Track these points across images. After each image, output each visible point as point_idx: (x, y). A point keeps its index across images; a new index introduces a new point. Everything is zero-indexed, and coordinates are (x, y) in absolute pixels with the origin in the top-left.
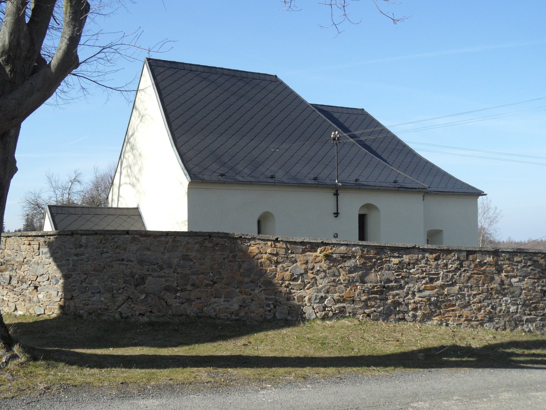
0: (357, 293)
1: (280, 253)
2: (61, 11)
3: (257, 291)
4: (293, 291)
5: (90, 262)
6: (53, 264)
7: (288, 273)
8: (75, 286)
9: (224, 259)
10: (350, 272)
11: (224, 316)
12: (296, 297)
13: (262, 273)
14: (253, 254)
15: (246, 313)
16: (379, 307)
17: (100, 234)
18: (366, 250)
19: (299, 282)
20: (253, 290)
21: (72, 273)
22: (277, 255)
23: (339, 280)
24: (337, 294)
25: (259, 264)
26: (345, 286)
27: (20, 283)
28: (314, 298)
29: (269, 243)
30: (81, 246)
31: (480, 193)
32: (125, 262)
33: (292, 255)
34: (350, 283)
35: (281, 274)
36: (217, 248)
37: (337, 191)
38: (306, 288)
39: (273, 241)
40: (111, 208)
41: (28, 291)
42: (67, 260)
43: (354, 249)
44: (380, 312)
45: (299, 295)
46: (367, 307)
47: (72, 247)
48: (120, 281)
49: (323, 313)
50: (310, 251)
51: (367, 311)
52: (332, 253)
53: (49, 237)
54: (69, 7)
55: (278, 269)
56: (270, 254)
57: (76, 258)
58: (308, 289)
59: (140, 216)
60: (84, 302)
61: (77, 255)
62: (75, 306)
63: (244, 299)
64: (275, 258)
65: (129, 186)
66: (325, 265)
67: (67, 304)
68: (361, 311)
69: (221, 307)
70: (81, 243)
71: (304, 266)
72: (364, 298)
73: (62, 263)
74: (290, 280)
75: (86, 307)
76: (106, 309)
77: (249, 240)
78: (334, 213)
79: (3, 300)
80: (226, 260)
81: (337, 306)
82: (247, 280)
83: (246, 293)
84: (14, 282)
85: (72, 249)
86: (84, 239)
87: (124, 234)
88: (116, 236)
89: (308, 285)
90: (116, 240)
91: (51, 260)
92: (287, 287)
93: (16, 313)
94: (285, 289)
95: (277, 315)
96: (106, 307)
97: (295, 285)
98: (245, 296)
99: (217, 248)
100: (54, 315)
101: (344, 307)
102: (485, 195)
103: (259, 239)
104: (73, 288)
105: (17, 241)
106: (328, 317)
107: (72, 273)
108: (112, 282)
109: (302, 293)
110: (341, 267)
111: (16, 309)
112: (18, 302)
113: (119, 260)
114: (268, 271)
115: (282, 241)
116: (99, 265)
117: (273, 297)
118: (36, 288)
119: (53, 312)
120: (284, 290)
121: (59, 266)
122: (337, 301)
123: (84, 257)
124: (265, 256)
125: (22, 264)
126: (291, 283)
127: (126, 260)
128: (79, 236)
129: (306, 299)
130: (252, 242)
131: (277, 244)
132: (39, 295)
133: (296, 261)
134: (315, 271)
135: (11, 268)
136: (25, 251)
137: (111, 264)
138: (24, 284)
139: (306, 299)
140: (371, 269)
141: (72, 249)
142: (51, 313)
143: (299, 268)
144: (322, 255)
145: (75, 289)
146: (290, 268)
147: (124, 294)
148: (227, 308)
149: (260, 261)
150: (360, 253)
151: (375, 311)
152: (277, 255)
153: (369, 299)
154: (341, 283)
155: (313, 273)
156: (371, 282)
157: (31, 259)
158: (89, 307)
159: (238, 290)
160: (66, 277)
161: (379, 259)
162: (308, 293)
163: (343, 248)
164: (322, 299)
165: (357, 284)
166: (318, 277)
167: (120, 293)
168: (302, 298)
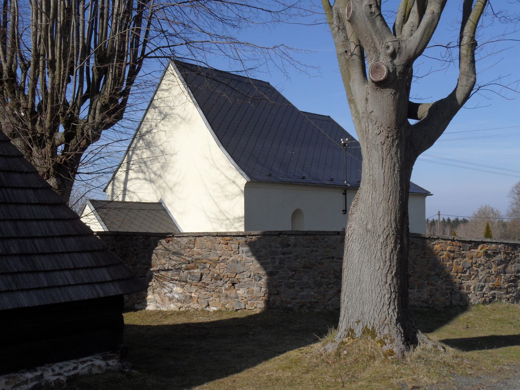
0: (502, 282)
1: (455, 250)
2: (9, 2)
3: (439, 283)
4: (463, 282)
5: (299, 260)
6: (256, 262)
7: (460, 266)
8: (281, 282)
9: (417, 256)
10: (498, 265)
11: (418, 304)
12: (465, 287)
13: (442, 268)
14: (437, 252)
15: (433, 301)
16: (514, 293)
17: (310, 235)
18: (506, 246)
19: (467, 274)
20: (437, 282)
21: (279, 270)
22: (453, 252)
23: (492, 272)
24: (491, 283)
25: (442, 260)
26: (495, 277)
27: (213, 280)
28: (477, 287)
29: (449, 242)
30: (289, 245)
31: (427, 194)
32: (335, 260)
33: (463, 252)
34: (498, 274)
35: (454, 267)
36: (412, 247)
37: (345, 191)
38: (472, 279)
39: (451, 240)
40: (118, 202)
41: (223, 288)
42: (273, 258)
43: (500, 246)
44: (514, 297)
45: (467, 285)
46: (508, 293)
47: (278, 246)
48: (330, 276)
49: (483, 299)
50: (474, 248)
51: (507, 296)
52: (488, 250)
53: (251, 237)
54: (470, 51)
55: (454, 264)
56: (449, 251)
57: (282, 256)
58: (473, 280)
59: (165, 210)
60: (292, 296)
61: (284, 254)
62: (282, 301)
63: (431, 289)
64: (452, 254)
65: (144, 181)
66: (483, 260)
67: (271, 299)
68: (504, 296)
69: (415, 296)
70: (289, 242)
71: (470, 261)
72: (506, 286)
73: (266, 261)
74: (462, 273)
75: (293, 301)
76: (317, 302)
77: (435, 239)
78: (343, 211)
79: (191, 297)
80: (419, 257)
81: (491, 293)
82: (433, 273)
83: (432, 285)
84: (205, 279)
85: (278, 248)
86: (292, 239)
87: (335, 235)
88: (327, 236)
89: (473, 277)
90: (326, 239)
91: (253, 258)
92: (460, 278)
93: (207, 309)
94: (459, 280)
95: (453, 301)
96: (316, 300)
97: (465, 276)
98: (431, 287)
99: (412, 247)
100: (258, 311)
101: (495, 294)
102: (432, 195)
103: (442, 239)
104: (280, 284)
105: (211, 241)
106: (486, 302)
107: (279, 270)
108: (322, 277)
109: (469, 283)
110: (493, 261)
111: (208, 305)
112: (211, 299)
113: (329, 258)
114: (447, 266)
115: (457, 240)
116: (310, 262)
117: (450, 287)
118: (233, 284)
119: (257, 306)
120: (458, 280)
121: (262, 264)
122: (492, 289)
123: (292, 255)
124: (445, 253)
125: (217, 262)
126: (462, 275)
127: (336, 258)
128: (285, 236)
129: (472, 288)
130: (437, 241)
131: (453, 242)
132: (238, 292)
133: (465, 257)
134: (477, 264)
135: (202, 266)
136: (221, 250)
137: (322, 261)
138: (219, 281)
139: (472, 288)
140: (509, 263)
141: (278, 248)
142: (253, 307)
143: (468, 261)
144: (482, 251)
145: (282, 285)
146: (461, 263)
147: (335, 288)
148: (420, 298)
149: (442, 257)
150: (503, 250)
151: (512, 296)
152: (453, 252)
153: (509, 287)
154: (493, 274)
155: (476, 267)
156: (509, 273)
157: (229, 258)
158: (297, 301)
159: (426, 282)
160: (270, 274)
161: (514, 254)
162: (472, 283)
163: (494, 245)
164: (483, 287)
165: (502, 274)
166: (479, 270)
167: (331, 288)
168: (468, 287)
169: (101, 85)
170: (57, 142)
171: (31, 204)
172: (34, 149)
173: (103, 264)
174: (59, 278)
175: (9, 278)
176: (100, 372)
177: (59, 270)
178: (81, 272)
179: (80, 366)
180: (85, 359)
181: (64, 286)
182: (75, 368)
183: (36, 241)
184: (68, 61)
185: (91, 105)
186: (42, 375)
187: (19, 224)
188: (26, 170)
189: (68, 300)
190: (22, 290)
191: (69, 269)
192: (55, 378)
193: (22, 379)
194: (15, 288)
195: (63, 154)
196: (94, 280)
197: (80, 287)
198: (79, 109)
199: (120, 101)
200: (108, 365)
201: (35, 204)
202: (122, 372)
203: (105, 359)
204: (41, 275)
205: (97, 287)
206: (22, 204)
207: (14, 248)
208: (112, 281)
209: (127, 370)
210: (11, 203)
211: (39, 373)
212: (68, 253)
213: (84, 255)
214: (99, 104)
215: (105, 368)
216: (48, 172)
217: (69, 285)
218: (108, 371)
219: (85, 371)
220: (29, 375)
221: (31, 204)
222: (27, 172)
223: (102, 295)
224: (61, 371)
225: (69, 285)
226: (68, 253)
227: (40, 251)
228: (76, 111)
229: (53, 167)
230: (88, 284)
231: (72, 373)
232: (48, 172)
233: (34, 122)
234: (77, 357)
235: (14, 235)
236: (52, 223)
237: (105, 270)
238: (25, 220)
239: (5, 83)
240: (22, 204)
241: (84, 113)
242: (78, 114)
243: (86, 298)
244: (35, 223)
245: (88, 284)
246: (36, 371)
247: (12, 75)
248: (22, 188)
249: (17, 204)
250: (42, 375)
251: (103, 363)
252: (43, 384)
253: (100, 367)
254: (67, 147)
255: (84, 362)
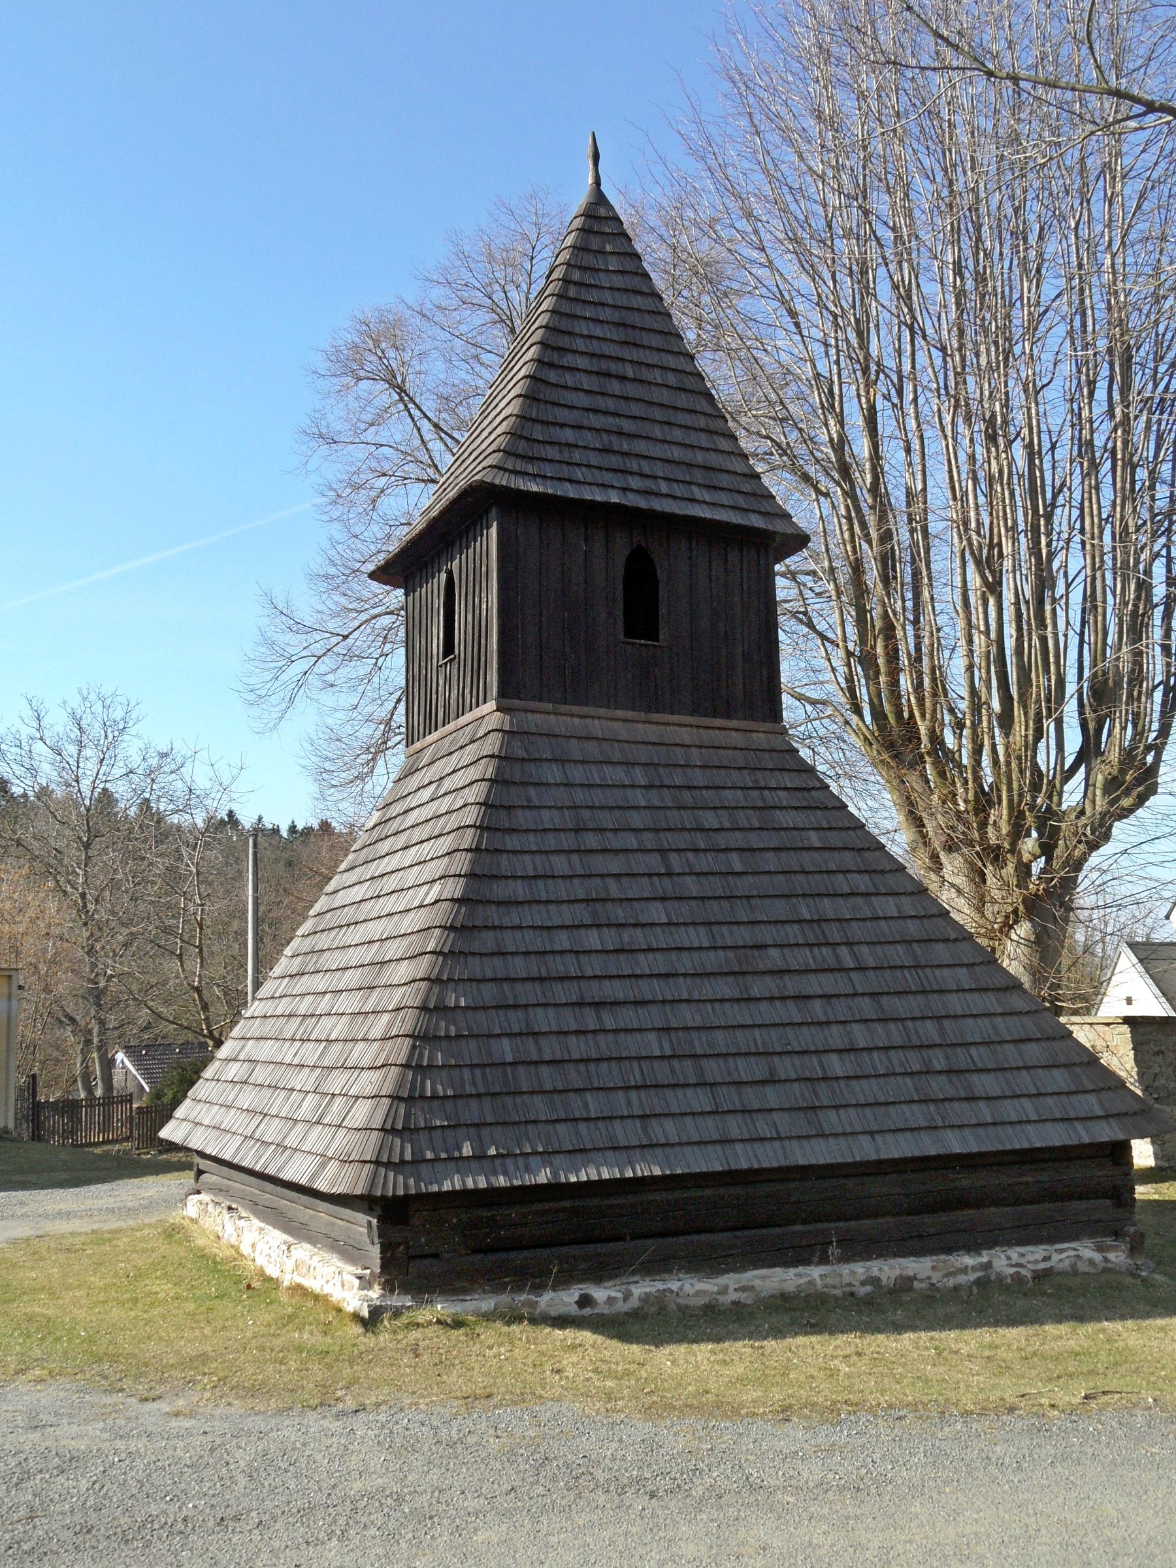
169: (1104, 739)
170: (1026, 857)
171: (964, 990)
172: (989, 870)
173: (1090, 1087)
174: (1010, 1108)
175: (932, 1107)
176: (1092, 1271)
177: (1011, 1097)
178: (1050, 1101)
179: (1056, 1257)
180: (1065, 1245)
181: (1020, 1122)
182: (1047, 1259)
183: (973, 1050)
184: (1032, 713)
185: (1087, 779)
186: (990, 1262)
187: (946, 1023)
188: (953, 936)
189: (1026, 1146)
190: (952, 1127)
191: (1029, 1096)
192: (1012, 1270)
193: (958, 1265)
194: (940, 1123)
195: (1040, 878)
196: (1072, 1115)
197: (1049, 1125)
198: (1060, 794)
199: (1150, 759)
200: (1106, 1260)
201: (971, 990)
202: (1134, 1276)
203: (1100, 1249)
204: (982, 1105)
205: (1078, 1126)
206: (950, 991)
207: (938, 1060)
208: (1106, 1117)
209: (1144, 1274)
210: (933, 992)
211: (985, 1259)
212: (1026, 1068)
213: (1055, 1072)
214: (1100, 777)
215: (1101, 1265)
216: (1015, 912)
217: (1029, 1122)
218: (1106, 1270)
219: (1066, 1264)
220: (969, 1260)
221: (964, 990)
222: (956, 940)
223: (1086, 1140)
224: (1023, 1261)
225: (1029, 1122)
226: (1026, 1068)
227: (980, 1065)
228: (1055, 799)
229: (1024, 901)
230: (1062, 1120)
231: (1042, 1266)
232: (1015, 912)
233: (983, 825)
234: (1051, 1240)
235: (938, 1042)
236: (998, 1021)
237: (1092, 1098)
238: (955, 1017)
239: (927, 758)
240: (950, 991)
241: (1073, 794)
242: (1060, 804)
243: (1058, 1144)
244: (970, 1022)
245: (1062, 1120)
246: (980, 1255)
247: (936, 740)
248: (949, 966)
249: (941, 991)
250: (990, 1262)
251: (1097, 1257)
252: (993, 1278)
253: (1091, 1262)
254: (1049, 861)
255: (1061, 1251)
